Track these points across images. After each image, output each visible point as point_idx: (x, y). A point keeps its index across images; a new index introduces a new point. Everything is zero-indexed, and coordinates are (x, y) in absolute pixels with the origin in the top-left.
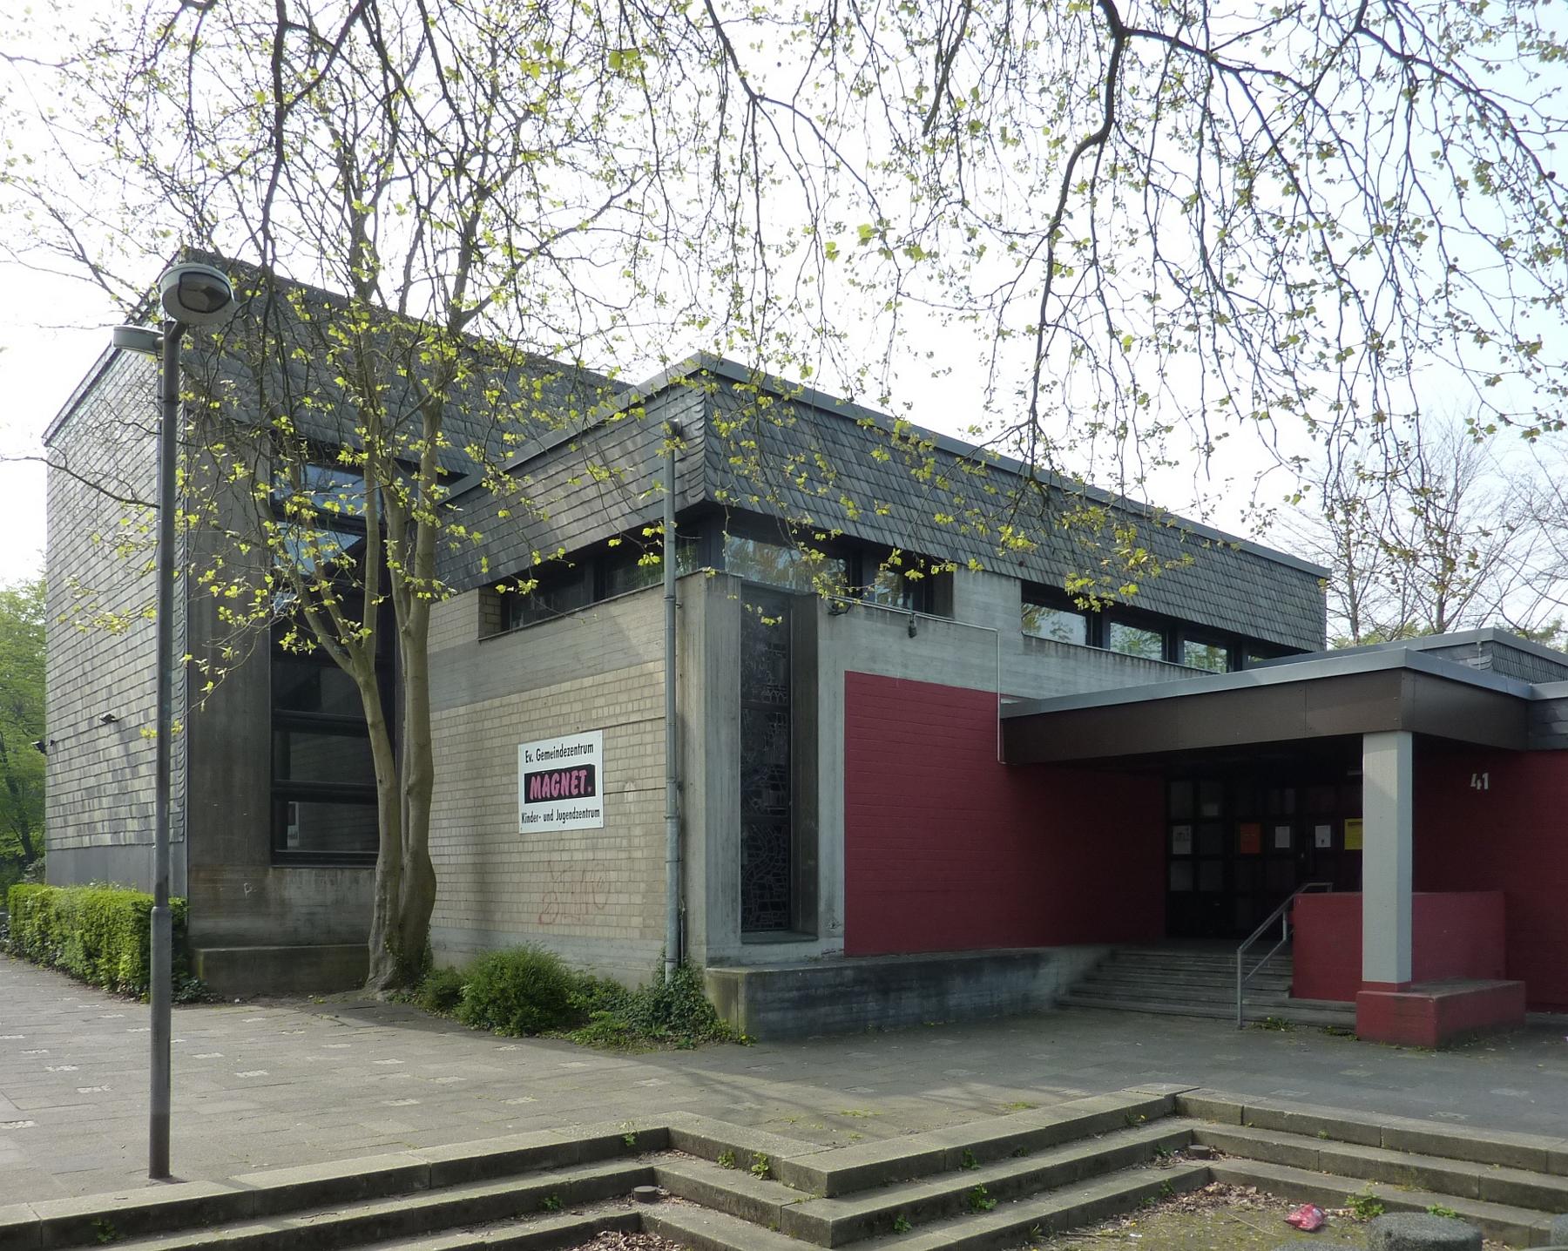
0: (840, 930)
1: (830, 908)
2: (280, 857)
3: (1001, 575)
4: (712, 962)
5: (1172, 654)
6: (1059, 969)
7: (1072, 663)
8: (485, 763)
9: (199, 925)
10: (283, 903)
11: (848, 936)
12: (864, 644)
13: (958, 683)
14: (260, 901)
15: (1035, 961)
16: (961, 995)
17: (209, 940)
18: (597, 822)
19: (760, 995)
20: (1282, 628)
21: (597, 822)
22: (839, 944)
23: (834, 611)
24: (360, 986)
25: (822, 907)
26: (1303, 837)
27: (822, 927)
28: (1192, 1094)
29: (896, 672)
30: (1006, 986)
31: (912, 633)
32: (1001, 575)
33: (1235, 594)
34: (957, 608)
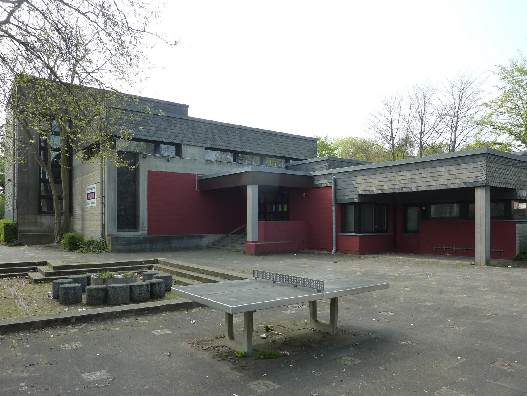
0: (146, 229)
1: (143, 224)
2: (40, 212)
3: (198, 146)
4: (108, 235)
5: (262, 163)
6: (208, 239)
7: (222, 166)
8: (83, 190)
9: (20, 228)
10: (42, 223)
11: (148, 231)
12: (149, 165)
13: (184, 172)
14: (35, 223)
15: (201, 237)
16: (176, 244)
17: (22, 232)
18: (95, 205)
19: (115, 242)
20: (299, 154)
21: (95, 205)
22: (146, 232)
23: (144, 157)
24: (53, 242)
25: (141, 224)
26: (277, 208)
27: (140, 228)
28: (161, 259)
29: (162, 170)
30: (196, 241)
31: (168, 161)
32: (198, 146)
33: (281, 146)
34: (183, 154)
